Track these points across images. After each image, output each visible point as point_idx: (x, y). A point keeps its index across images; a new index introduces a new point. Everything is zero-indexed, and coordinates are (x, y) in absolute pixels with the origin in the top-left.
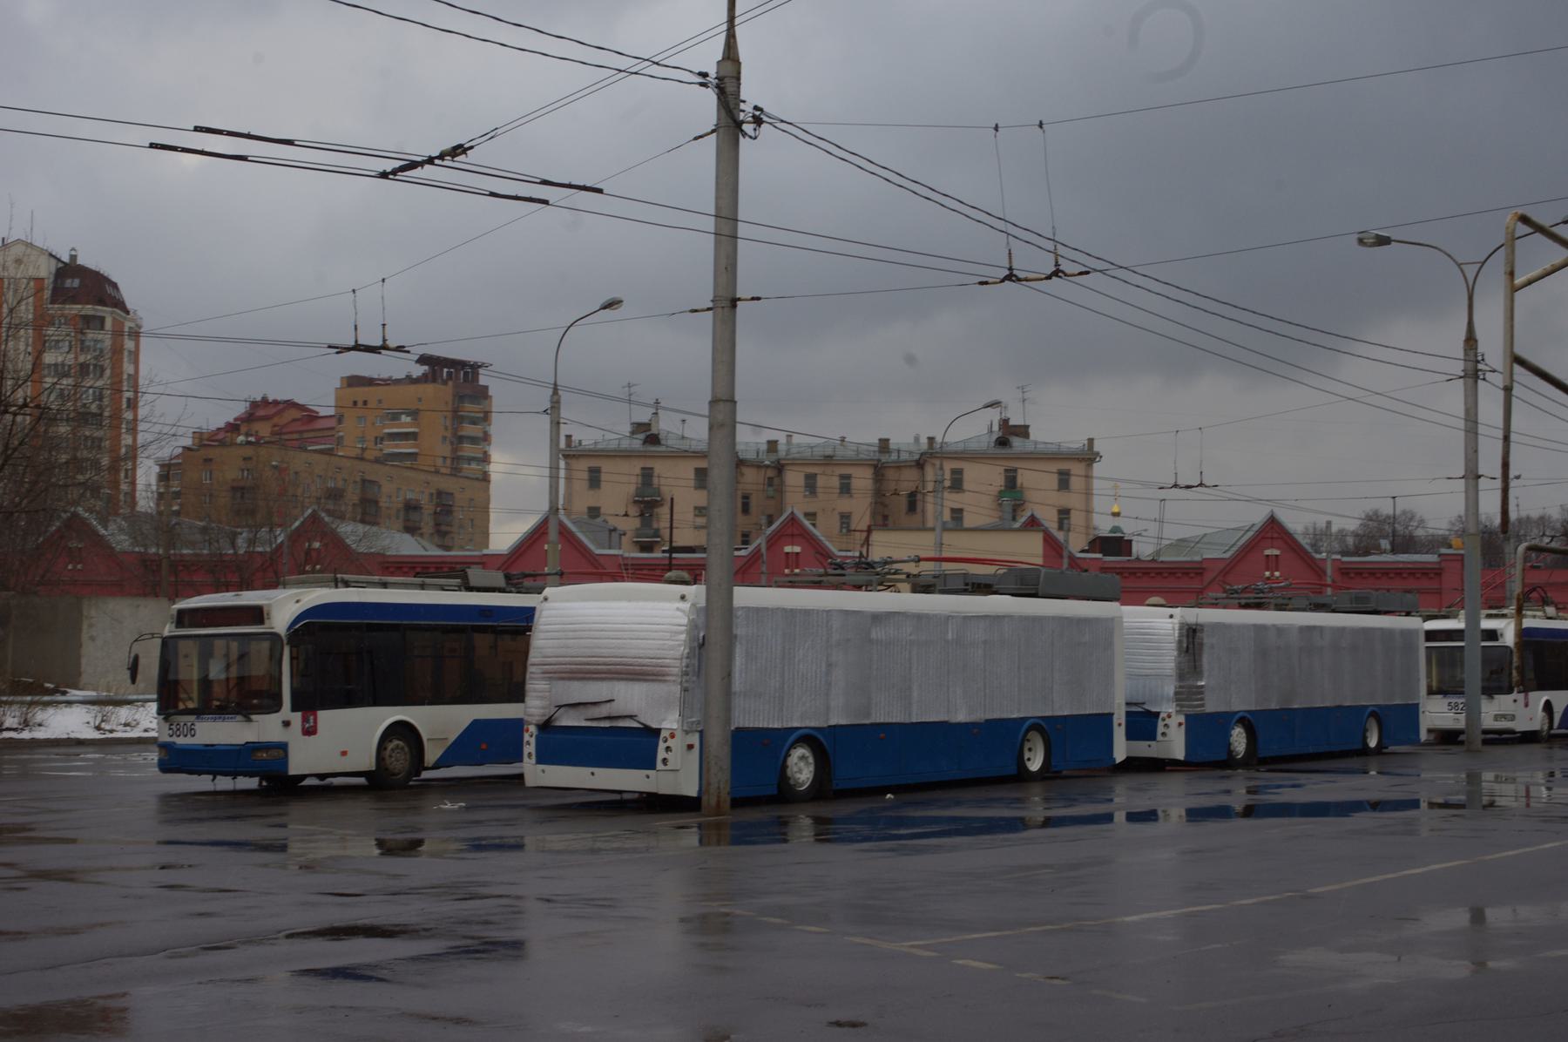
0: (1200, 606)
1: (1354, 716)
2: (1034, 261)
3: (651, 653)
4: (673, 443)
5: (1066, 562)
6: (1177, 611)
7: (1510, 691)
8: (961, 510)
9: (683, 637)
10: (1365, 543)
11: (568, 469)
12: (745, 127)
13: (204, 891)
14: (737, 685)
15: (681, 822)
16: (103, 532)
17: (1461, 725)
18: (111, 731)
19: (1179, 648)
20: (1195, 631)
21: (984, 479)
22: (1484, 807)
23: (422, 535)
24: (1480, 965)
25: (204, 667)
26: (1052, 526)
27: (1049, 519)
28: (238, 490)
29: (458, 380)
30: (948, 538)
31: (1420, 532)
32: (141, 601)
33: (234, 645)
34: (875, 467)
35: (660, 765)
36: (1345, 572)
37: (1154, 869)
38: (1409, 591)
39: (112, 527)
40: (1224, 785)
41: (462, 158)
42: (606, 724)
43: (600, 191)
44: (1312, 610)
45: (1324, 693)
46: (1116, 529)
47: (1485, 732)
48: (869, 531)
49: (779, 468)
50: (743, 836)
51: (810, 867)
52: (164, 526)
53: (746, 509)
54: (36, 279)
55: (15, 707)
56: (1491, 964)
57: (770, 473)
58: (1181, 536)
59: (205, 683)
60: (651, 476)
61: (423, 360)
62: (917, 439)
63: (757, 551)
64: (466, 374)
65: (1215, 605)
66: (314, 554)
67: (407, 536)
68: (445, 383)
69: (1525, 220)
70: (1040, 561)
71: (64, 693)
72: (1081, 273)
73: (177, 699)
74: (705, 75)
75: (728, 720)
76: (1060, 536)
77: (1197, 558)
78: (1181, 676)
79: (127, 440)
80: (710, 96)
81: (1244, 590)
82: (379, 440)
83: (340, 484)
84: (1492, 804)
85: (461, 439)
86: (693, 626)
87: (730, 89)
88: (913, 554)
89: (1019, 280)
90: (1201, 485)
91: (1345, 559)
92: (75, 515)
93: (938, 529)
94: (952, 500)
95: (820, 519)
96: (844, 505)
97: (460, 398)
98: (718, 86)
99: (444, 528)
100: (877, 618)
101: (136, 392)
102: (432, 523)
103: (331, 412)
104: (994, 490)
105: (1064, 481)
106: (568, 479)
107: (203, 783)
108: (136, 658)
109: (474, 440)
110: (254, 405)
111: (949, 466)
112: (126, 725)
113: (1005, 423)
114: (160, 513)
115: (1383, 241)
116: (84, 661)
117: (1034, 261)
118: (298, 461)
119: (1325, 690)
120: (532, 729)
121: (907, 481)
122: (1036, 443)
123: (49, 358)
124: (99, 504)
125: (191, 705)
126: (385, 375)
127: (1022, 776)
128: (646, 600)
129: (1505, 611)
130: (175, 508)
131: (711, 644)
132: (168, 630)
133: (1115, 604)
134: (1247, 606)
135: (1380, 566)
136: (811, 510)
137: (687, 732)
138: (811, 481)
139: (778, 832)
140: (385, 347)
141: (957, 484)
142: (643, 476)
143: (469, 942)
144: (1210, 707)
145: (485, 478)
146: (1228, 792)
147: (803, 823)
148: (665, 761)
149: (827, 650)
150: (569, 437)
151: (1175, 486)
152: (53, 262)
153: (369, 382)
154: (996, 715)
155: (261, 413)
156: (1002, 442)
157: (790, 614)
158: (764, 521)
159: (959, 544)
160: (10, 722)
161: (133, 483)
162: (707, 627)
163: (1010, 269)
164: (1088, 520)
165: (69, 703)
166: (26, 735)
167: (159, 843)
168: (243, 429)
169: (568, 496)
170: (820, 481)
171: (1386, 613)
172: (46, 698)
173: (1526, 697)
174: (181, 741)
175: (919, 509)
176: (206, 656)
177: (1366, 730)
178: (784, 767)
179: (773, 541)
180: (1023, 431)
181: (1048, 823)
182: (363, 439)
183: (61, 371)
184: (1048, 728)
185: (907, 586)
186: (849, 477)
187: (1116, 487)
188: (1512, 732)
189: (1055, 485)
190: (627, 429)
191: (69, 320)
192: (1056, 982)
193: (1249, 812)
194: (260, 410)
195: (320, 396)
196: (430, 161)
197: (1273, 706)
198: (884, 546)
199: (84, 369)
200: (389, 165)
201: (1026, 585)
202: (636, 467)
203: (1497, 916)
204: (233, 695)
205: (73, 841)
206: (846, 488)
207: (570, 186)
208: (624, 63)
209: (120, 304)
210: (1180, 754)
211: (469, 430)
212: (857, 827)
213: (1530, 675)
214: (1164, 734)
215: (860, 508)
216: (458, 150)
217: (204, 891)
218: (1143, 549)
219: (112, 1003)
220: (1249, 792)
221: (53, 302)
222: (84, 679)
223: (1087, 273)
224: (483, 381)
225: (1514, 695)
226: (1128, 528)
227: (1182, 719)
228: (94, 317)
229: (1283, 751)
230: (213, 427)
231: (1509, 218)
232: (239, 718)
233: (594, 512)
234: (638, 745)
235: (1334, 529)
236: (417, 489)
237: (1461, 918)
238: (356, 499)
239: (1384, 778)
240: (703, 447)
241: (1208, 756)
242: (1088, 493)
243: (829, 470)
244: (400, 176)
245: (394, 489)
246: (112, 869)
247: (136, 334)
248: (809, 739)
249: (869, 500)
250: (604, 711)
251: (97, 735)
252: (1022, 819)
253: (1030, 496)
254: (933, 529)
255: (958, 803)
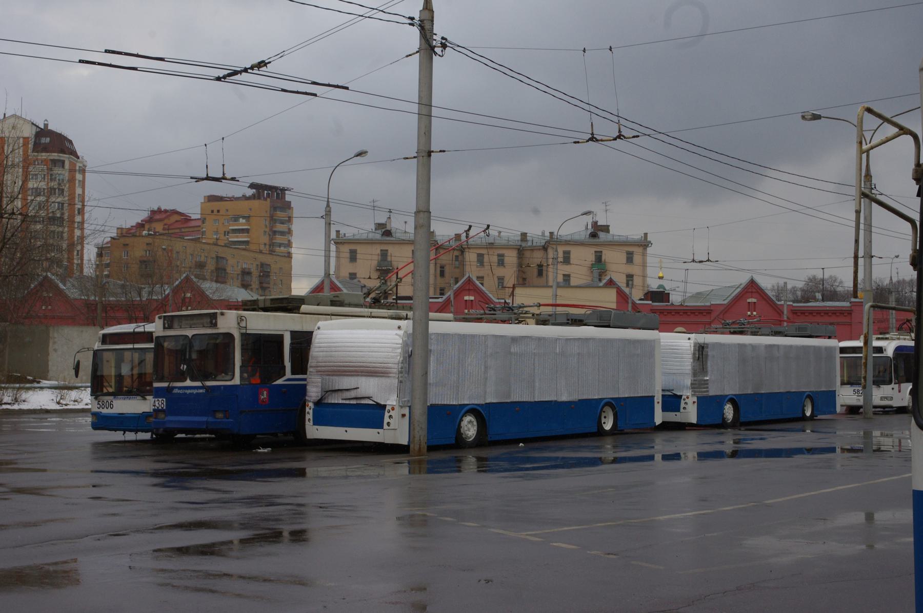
0: (706, 332)
1: (798, 398)
2: (606, 129)
3: (381, 360)
4: (398, 235)
5: (630, 305)
6: (692, 336)
7: (890, 383)
8: (569, 276)
9: (399, 351)
10: (807, 296)
11: (338, 251)
12: (436, 49)
13: (113, 500)
14: (431, 378)
15: (398, 460)
16: (61, 286)
17: (861, 403)
18: (66, 405)
19: (694, 358)
20: (703, 348)
21: (583, 257)
22: (874, 451)
23: (252, 290)
24: (871, 547)
25: (118, 367)
26: (623, 285)
27: (621, 280)
28: (143, 262)
29: (272, 197)
30: (560, 292)
31: (839, 289)
32: (85, 329)
33: (136, 355)
34: (519, 249)
35: (385, 426)
36: (795, 312)
37: (677, 488)
38: (831, 324)
39: (69, 284)
40: (721, 438)
41: (264, 68)
42: (354, 402)
43: (347, 88)
44: (772, 335)
45: (779, 385)
46: (661, 286)
47: (875, 407)
48: (514, 287)
49: (462, 250)
50: (434, 469)
51: (473, 485)
52: (99, 284)
53: (442, 274)
54: (24, 138)
55: (10, 390)
56: (864, 547)
57: (456, 253)
58: (699, 291)
59: (119, 378)
60: (386, 255)
61: (252, 186)
62: (543, 233)
63: (449, 299)
64: (278, 194)
65: (715, 332)
66: (187, 300)
67: (243, 290)
68: (265, 199)
69: (869, 110)
70: (614, 306)
71: (39, 382)
72: (634, 137)
73: (102, 386)
74: (412, 19)
75: (426, 400)
76: (627, 290)
77: (708, 304)
78: (695, 374)
79: (77, 233)
80: (415, 31)
81: (733, 323)
82: (226, 233)
83: (203, 259)
84: (879, 450)
85: (275, 232)
86: (405, 345)
87: (427, 26)
88: (536, 301)
89: (597, 140)
90: (708, 260)
91: (795, 305)
92: (46, 277)
93: (554, 287)
94: (564, 269)
95: (485, 282)
96: (500, 272)
97: (275, 209)
98: (420, 25)
99: (265, 285)
100: (515, 340)
101: (83, 206)
102: (257, 282)
103: (199, 216)
104: (588, 263)
105: (630, 259)
106: (338, 257)
107: (118, 436)
108: (78, 362)
109: (282, 233)
110: (153, 212)
111: (561, 250)
112: (75, 401)
113: (595, 224)
114: (97, 276)
115: (816, 117)
116: (50, 363)
117: (606, 129)
118: (178, 245)
119: (780, 382)
120: (311, 405)
121: (537, 257)
122: (613, 236)
123: (31, 184)
124: (61, 271)
125: (111, 390)
126: (230, 195)
127: (600, 433)
128: (361, 328)
129: (887, 336)
130: (106, 273)
131: (416, 354)
132: (97, 346)
133: (656, 332)
134: (734, 333)
135: (816, 309)
136: (481, 275)
137: (402, 407)
138: (480, 257)
139: (456, 466)
140: (224, 178)
141: (567, 260)
142: (382, 255)
143: (267, 531)
144: (712, 393)
145: (289, 256)
146: (722, 443)
147: (470, 460)
148: (388, 424)
149: (482, 360)
150: (338, 232)
151: (693, 261)
152: (35, 128)
153: (220, 199)
154: (585, 397)
155: (157, 217)
156: (594, 235)
157: (463, 337)
158: (452, 281)
159: (567, 296)
160: (6, 399)
161: (82, 259)
162: (413, 346)
163: (592, 134)
164: (644, 281)
165: (42, 388)
166: (16, 407)
167: (92, 471)
168: (147, 226)
169: (338, 267)
170: (486, 258)
171: (817, 337)
172: (28, 385)
173: (899, 387)
174: (105, 411)
175: (544, 273)
176: (119, 362)
177: (804, 406)
178: (459, 426)
179: (458, 293)
180: (606, 229)
181: (616, 461)
182: (217, 232)
183: (37, 192)
184: (614, 404)
185: (534, 321)
186: (503, 255)
187: (661, 262)
188: (891, 407)
189: (624, 261)
190: (373, 227)
191: (44, 162)
192: (611, 556)
193: (735, 454)
194: (156, 215)
195: (193, 208)
196: (246, 70)
197: (749, 392)
198: (524, 297)
199: (52, 191)
200: (221, 73)
201: (603, 320)
202: (376, 250)
203: (881, 517)
204: (136, 384)
205: (45, 470)
206: (501, 263)
207: (329, 85)
208: (362, 11)
209: (74, 153)
210: (693, 419)
211: (279, 227)
212: (502, 463)
213: (902, 373)
214: (684, 408)
215: (509, 274)
216: (262, 64)
217: (113, 500)
218: (676, 299)
219: (66, 567)
220: (735, 442)
221: (33, 151)
222: (51, 374)
223: (638, 136)
224: (288, 198)
225: (893, 385)
226: (668, 286)
227: (695, 399)
228: (59, 160)
229: (755, 418)
230: (128, 226)
231: (859, 109)
232: (139, 397)
233: (353, 276)
234: (373, 414)
235: (789, 287)
236: (249, 262)
237: (860, 517)
238: (213, 268)
239: (815, 435)
240: (412, 237)
241: (710, 421)
242: (644, 265)
243: (491, 252)
244: (228, 79)
245: (235, 263)
246: (60, 487)
247: (83, 171)
248: (474, 411)
249: (515, 269)
250: (353, 394)
251: (58, 407)
252: (600, 458)
253: (611, 267)
254: (551, 287)
255: (561, 449)
